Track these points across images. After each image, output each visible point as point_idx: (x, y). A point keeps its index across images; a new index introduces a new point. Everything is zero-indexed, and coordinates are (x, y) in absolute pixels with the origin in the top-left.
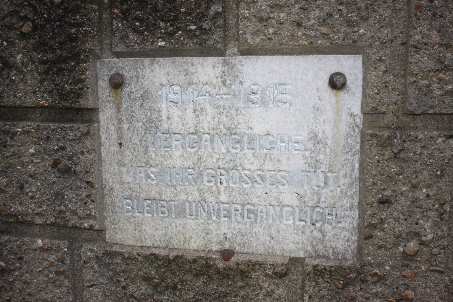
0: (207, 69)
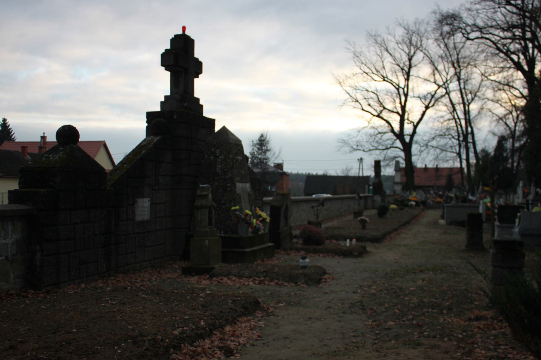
0: (142, 199)
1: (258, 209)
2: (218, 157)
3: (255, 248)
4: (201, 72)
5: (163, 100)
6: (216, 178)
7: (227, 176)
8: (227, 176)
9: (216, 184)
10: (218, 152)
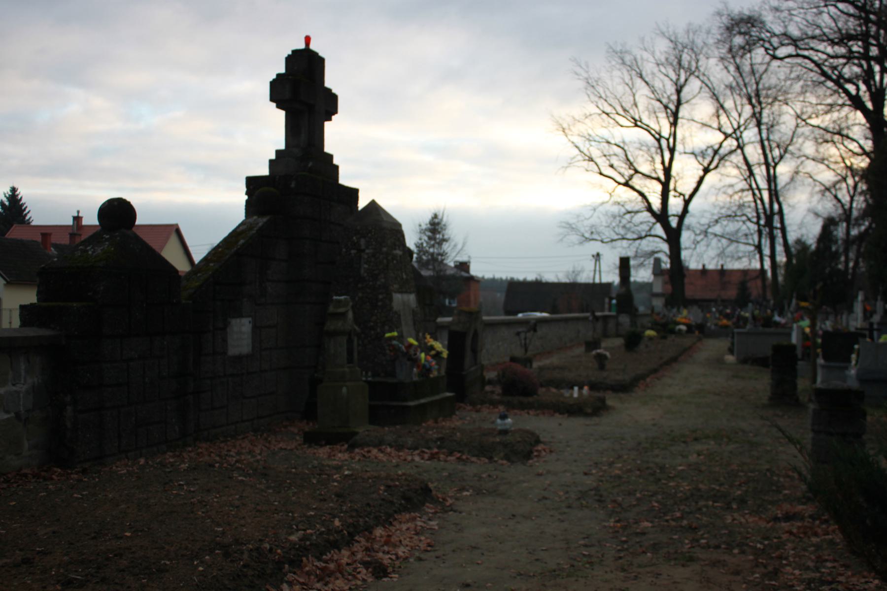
1: (428, 337)
2: (363, 251)
3: (423, 401)
4: (335, 111)
5: (273, 157)
6: (360, 285)
7: (378, 283)
8: (378, 283)
9: (360, 295)
10: (363, 242)
